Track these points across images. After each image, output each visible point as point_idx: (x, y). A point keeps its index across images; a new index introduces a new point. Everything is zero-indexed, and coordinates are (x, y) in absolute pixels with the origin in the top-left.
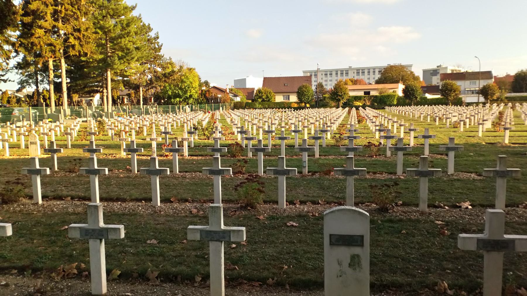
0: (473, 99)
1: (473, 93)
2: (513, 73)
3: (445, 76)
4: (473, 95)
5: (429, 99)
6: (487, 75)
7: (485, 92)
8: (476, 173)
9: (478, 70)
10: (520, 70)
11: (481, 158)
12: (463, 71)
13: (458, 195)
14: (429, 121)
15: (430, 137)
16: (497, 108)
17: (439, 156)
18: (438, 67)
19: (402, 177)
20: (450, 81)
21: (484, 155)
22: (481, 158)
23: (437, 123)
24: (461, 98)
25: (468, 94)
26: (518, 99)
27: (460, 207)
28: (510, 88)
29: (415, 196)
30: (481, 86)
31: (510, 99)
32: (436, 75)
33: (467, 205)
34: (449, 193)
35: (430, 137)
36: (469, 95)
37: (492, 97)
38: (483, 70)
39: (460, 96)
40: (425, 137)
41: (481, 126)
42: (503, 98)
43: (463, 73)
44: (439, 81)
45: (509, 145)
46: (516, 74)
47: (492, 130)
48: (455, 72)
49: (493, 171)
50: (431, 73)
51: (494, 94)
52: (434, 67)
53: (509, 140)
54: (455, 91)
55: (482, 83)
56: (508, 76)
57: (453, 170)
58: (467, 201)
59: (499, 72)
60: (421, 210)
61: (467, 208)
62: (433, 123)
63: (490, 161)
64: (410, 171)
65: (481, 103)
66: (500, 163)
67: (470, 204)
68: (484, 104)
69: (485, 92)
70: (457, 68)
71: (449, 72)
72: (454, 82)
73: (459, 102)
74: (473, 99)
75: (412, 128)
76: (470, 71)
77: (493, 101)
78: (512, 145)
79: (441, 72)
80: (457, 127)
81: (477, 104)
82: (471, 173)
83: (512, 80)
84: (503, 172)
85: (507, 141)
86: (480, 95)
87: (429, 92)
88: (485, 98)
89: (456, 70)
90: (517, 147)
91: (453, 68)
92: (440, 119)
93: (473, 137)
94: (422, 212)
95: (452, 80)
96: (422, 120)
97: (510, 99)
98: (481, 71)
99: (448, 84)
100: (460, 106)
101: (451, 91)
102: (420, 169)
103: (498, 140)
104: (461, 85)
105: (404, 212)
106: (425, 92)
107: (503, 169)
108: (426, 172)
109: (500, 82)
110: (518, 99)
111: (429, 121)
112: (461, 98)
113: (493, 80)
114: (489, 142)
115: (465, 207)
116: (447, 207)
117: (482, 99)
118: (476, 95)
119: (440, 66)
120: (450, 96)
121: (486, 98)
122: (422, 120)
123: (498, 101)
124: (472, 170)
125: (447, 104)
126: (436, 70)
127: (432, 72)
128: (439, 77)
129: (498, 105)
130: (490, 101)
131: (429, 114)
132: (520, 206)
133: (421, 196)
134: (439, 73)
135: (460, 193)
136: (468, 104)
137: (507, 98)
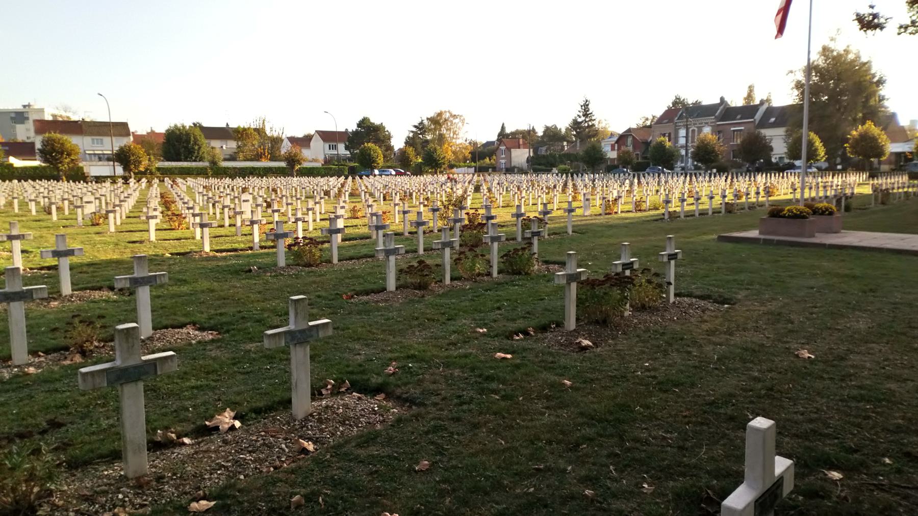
0: (104, 169)
1: (100, 159)
2: (161, 129)
3: (43, 126)
4: (101, 163)
5: (17, 168)
6: (121, 129)
7: (123, 157)
8: (194, 324)
9: (108, 120)
10: (173, 125)
11: (185, 289)
12: (74, 118)
13: (195, 397)
14: (34, 213)
15: (70, 253)
16: (137, 185)
17: (97, 295)
18: (25, 106)
19: (32, 370)
20: (59, 136)
21: (185, 282)
22: (185, 289)
23: (55, 217)
24: (82, 168)
25: (91, 160)
26: (176, 172)
27: (216, 428)
28: (160, 152)
29: (94, 428)
30: (116, 149)
31: (165, 172)
32: (23, 123)
33: (226, 419)
34: (170, 394)
35: (70, 253)
36: (94, 163)
37: (136, 167)
38: (115, 119)
39: (81, 165)
40: (57, 254)
41: (79, 210)
42: (154, 170)
43: (76, 122)
44: (32, 133)
45: (211, 254)
46: (167, 131)
47: (165, 226)
48: (60, 119)
49: (285, 332)
50: (12, 118)
51: (140, 162)
52: (17, 106)
53: (398, 279)
54: (69, 155)
55: (118, 143)
56: (152, 133)
57: (150, 326)
58: (224, 410)
59: (139, 127)
60: (130, 475)
61: (232, 428)
62: (43, 216)
63: (203, 292)
64: (92, 373)
65: (119, 177)
66: (296, 314)
67: (233, 414)
68: (126, 180)
69: (123, 157)
70: (64, 114)
71: (48, 117)
72: (65, 137)
73: (78, 176)
74: (104, 169)
75: (15, 232)
76: (87, 120)
77: (139, 176)
78: (218, 254)
79: (33, 117)
80: (98, 224)
81: (113, 179)
82: (182, 326)
83: (162, 140)
84: (302, 332)
85: (207, 249)
86: (116, 163)
87: (16, 155)
88: (125, 169)
89: (61, 116)
90: (225, 258)
91: (57, 112)
92: (58, 208)
93: (141, 242)
94: (138, 479)
95: (61, 132)
96: (16, 211)
97: (165, 172)
98: (113, 120)
99: (54, 140)
100: (74, 181)
101: (62, 153)
102: (118, 363)
103: (188, 247)
104: (80, 143)
105: (86, 499)
106: (8, 153)
107: (302, 326)
108: (135, 367)
109: (144, 141)
110: (176, 172)
111: (34, 213)
112: (82, 168)
113: (131, 138)
114: (174, 251)
115: (227, 426)
116: (187, 440)
117: (120, 170)
118: (106, 163)
119: (29, 106)
120: (61, 162)
121: (126, 168)
122: (16, 211)
123: (147, 173)
124: (183, 320)
125: (57, 179)
126: (22, 113)
127: (13, 115)
128: (30, 125)
129: (571, 211)
130: (135, 173)
131: (15, 195)
132: (324, 392)
133: (128, 436)
134: (27, 118)
135: (197, 387)
136: (99, 179)
137: (158, 169)
